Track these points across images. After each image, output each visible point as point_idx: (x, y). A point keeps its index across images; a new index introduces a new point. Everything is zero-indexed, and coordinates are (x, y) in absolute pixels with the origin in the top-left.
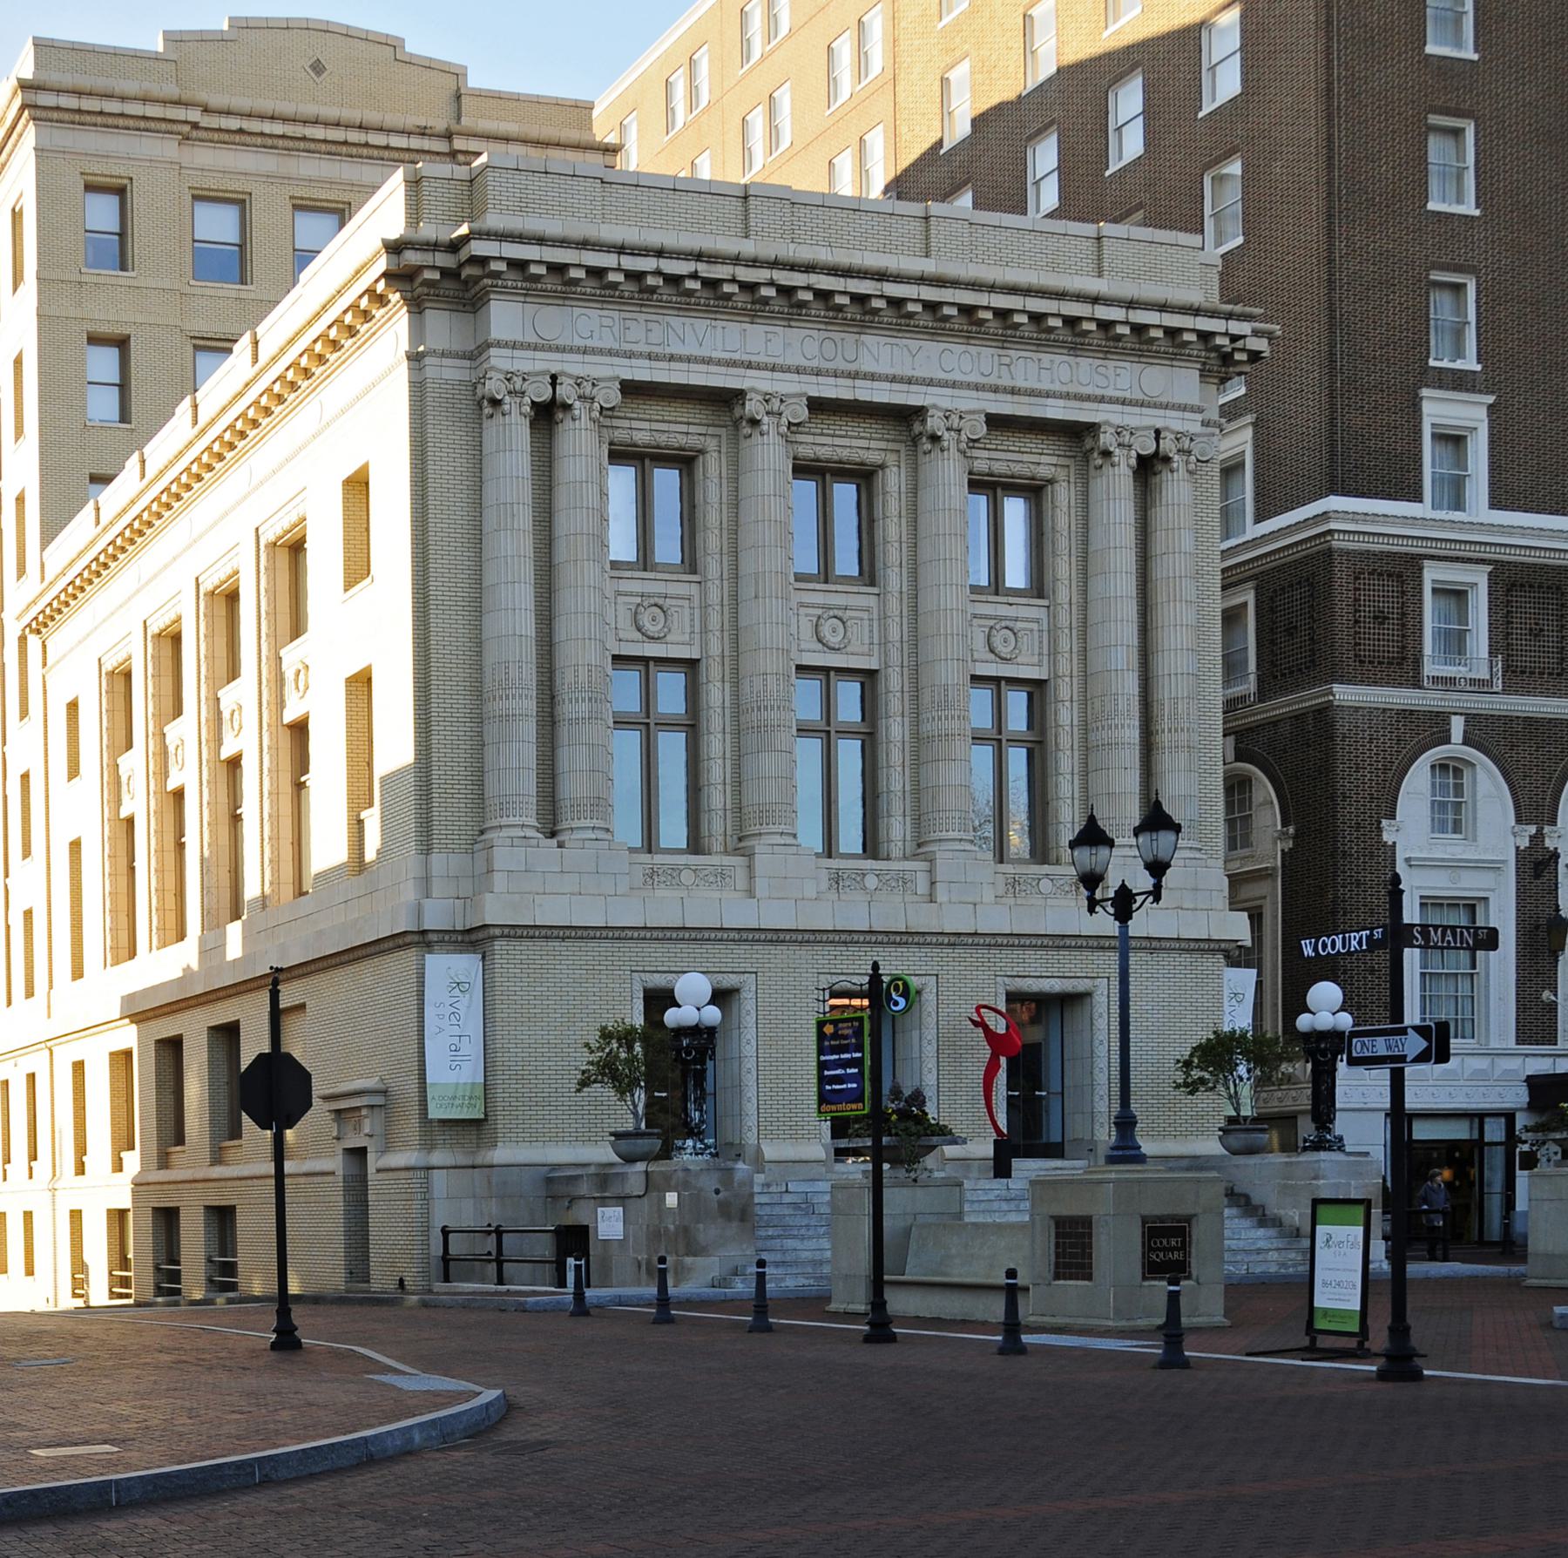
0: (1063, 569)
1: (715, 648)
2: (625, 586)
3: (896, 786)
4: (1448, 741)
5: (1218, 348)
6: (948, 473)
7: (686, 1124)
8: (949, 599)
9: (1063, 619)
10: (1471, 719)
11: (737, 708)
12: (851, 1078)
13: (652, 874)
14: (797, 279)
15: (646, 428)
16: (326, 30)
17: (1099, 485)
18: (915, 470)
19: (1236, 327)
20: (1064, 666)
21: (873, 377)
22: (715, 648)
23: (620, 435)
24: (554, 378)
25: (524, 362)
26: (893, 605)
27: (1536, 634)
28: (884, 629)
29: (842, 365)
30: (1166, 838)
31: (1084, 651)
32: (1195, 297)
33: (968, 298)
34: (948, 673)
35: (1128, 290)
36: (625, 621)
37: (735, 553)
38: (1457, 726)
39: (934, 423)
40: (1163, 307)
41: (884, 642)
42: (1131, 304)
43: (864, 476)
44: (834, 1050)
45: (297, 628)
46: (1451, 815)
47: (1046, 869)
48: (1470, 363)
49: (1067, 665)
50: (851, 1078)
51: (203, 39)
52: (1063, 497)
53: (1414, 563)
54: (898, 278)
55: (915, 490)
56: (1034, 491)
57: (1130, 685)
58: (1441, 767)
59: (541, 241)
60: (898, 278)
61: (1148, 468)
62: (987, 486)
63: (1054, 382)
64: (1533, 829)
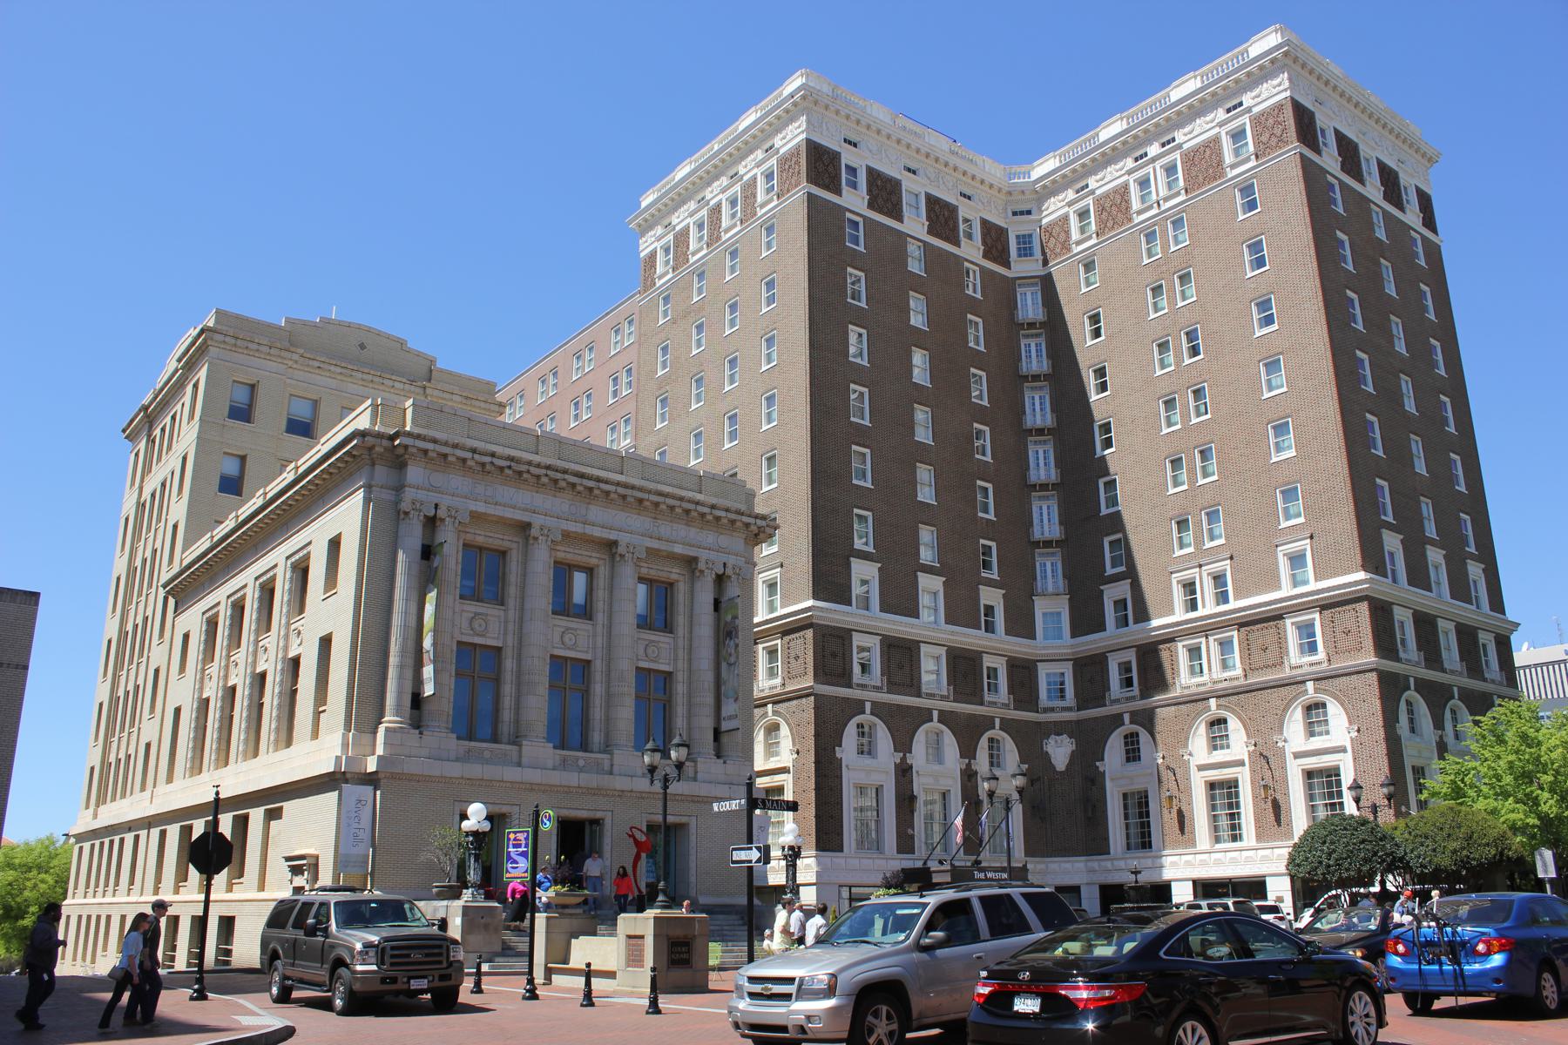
1: (510, 643)
2: (467, 608)
10: (941, 712)
11: (519, 673)
13: (564, 760)
16: (369, 330)
17: (698, 585)
18: (613, 567)
20: (680, 665)
22: (510, 643)
23: (469, 537)
24: (436, 506)
25: (421, 495)
26: (599, 628)
27: (901, 667)
31: (690, 660)
33: (640, 495)
36: (465, 624)
37: (523, 598)
41: (594, 648)
45: (302, 610)
46: (866, 750)
49: (511, 641)
51: (305, 324)
55: (612, 577)
56: (590, 571)
58: (860, 726)
59: (435, 441)
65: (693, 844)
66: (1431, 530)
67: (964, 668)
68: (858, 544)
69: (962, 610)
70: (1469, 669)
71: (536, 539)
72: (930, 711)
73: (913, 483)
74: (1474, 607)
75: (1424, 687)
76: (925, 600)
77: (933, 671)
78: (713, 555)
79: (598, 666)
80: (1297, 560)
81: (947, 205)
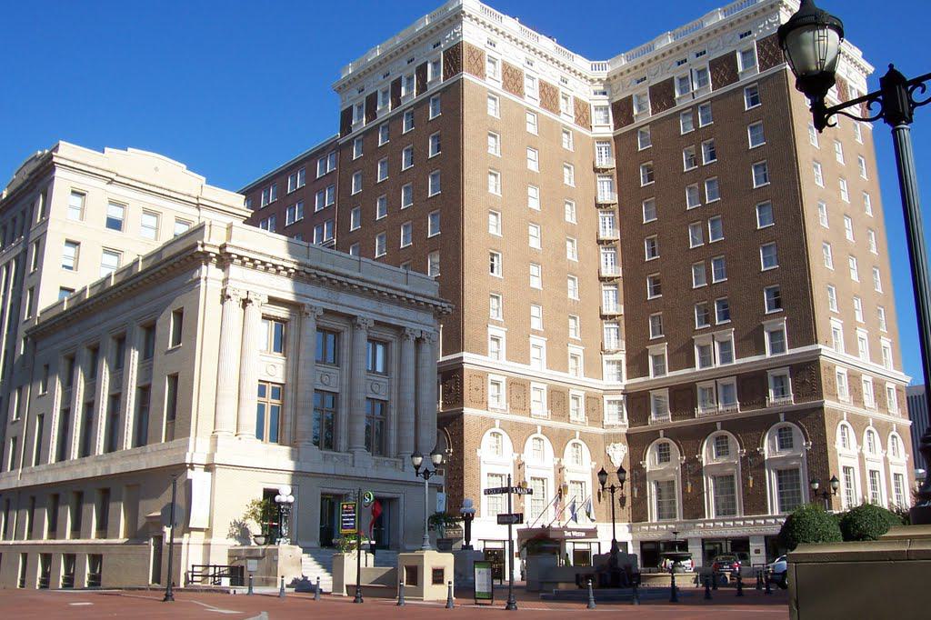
0: (394, 368)
1: (344, 389)
3: (343, 429)
4: (494, 427)
5: (438, 310)
6: (362, 336)
7: (281, 534)
8: (361, 373)
9: (393, 383)
10: (543, 427)
12: (351, 522)
14: (323, 274)
15: (376, 334)
19: (443, 305)
20: (393, 396)
21: (342, 305)
28: (390, 389)
29: (334, 300)
30: (604, 477)
32: (430, 294)
34: (361, 397)
35: (415, 290)
38: (539, 429)
39: (359, 321)
40: (424, 297)
41: (341, 385)
42: (416, 295)
43: (337, 334)
44: (346, 513)
46: (578, 459)
47: (387, 459)
48: (500, 319)
49: (394, 397)
50: (351, 522)
52: (394, 347)
53: (487, 374)
54: (352, 278)
56: (386, 344)
57: (412, 405)
60: (352, 278)
61: (419, 341)
62: (373, 341)
63: (394, 314)
64: (518, 455)
65: (401, 511)
66: (859, 318)
67: (558, 399)
68: (493, 314)
69: (558, 359)
70: (880, 407)
71: (307, 314)
72: (536, 426)
73: (528, 275)
74: (833, 350)
75: (877, 424)
76: (534, 352)
77: (539, 402)
78: (415, 326)
79: (344, 396)
80: (776, 335)
81: (552, 88)
